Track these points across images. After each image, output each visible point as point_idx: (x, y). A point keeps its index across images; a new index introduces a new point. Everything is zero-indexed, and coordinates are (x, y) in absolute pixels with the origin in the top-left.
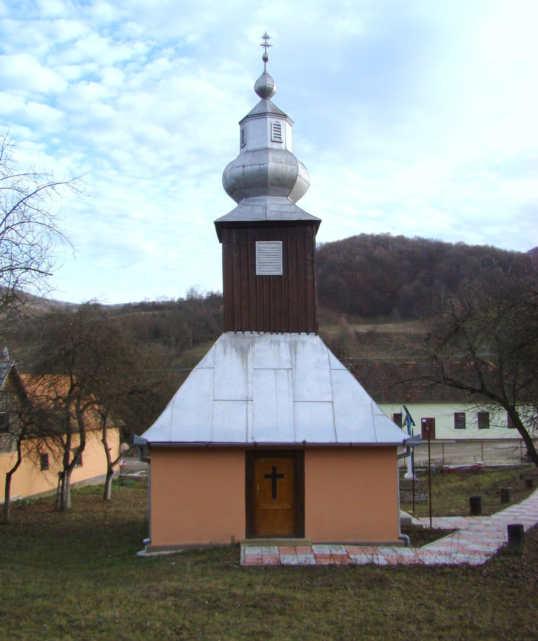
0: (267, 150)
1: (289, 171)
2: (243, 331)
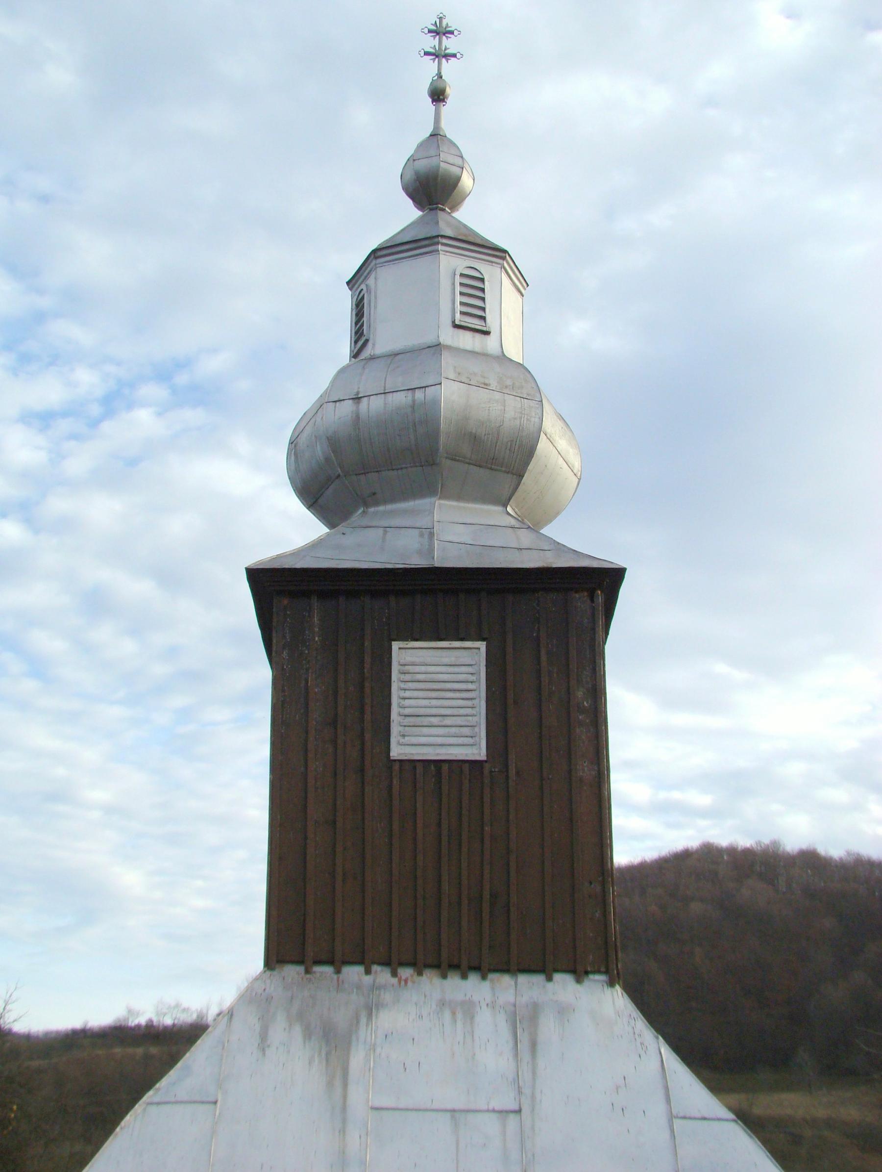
0: (437, 348)
1: (510, 414)
2: (337, 962)
